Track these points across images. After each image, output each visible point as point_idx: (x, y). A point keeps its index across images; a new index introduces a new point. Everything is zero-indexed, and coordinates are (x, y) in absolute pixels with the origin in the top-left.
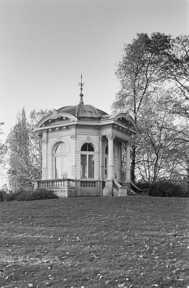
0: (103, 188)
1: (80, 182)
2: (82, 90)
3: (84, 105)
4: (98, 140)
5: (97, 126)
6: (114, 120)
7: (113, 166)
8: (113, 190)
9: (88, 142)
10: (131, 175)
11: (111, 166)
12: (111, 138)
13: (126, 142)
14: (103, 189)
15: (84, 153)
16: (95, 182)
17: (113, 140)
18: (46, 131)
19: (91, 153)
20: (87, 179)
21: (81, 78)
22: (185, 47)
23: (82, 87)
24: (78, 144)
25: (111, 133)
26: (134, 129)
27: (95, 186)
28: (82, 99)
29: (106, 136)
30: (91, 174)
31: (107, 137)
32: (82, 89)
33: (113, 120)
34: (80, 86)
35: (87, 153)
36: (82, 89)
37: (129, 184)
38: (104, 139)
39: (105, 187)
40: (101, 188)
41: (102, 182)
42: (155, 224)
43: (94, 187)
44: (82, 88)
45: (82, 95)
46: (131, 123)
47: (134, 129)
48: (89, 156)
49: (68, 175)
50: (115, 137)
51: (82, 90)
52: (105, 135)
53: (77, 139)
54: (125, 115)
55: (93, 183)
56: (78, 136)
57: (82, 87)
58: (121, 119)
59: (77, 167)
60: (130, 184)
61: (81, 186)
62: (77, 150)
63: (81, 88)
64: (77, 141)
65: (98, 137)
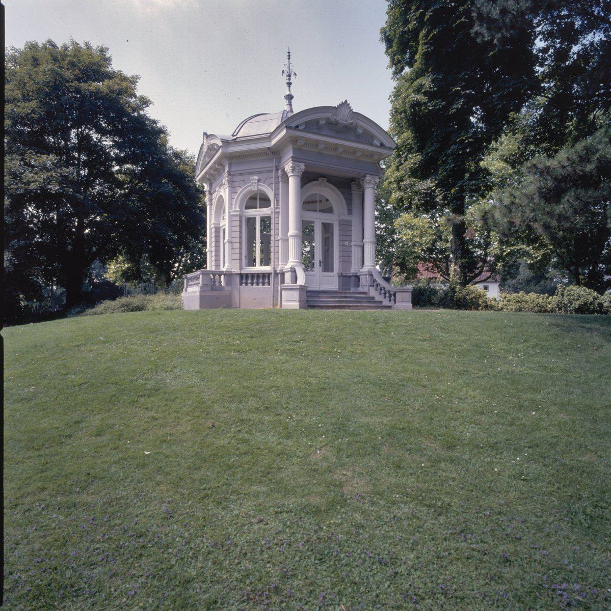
19: (266, 212)
20: (258, 268)
21: (289, 59)
27: (269, 284)
43: (266, 286)
57: (290, 79)
58: (322, 122)
61: (241, 284)
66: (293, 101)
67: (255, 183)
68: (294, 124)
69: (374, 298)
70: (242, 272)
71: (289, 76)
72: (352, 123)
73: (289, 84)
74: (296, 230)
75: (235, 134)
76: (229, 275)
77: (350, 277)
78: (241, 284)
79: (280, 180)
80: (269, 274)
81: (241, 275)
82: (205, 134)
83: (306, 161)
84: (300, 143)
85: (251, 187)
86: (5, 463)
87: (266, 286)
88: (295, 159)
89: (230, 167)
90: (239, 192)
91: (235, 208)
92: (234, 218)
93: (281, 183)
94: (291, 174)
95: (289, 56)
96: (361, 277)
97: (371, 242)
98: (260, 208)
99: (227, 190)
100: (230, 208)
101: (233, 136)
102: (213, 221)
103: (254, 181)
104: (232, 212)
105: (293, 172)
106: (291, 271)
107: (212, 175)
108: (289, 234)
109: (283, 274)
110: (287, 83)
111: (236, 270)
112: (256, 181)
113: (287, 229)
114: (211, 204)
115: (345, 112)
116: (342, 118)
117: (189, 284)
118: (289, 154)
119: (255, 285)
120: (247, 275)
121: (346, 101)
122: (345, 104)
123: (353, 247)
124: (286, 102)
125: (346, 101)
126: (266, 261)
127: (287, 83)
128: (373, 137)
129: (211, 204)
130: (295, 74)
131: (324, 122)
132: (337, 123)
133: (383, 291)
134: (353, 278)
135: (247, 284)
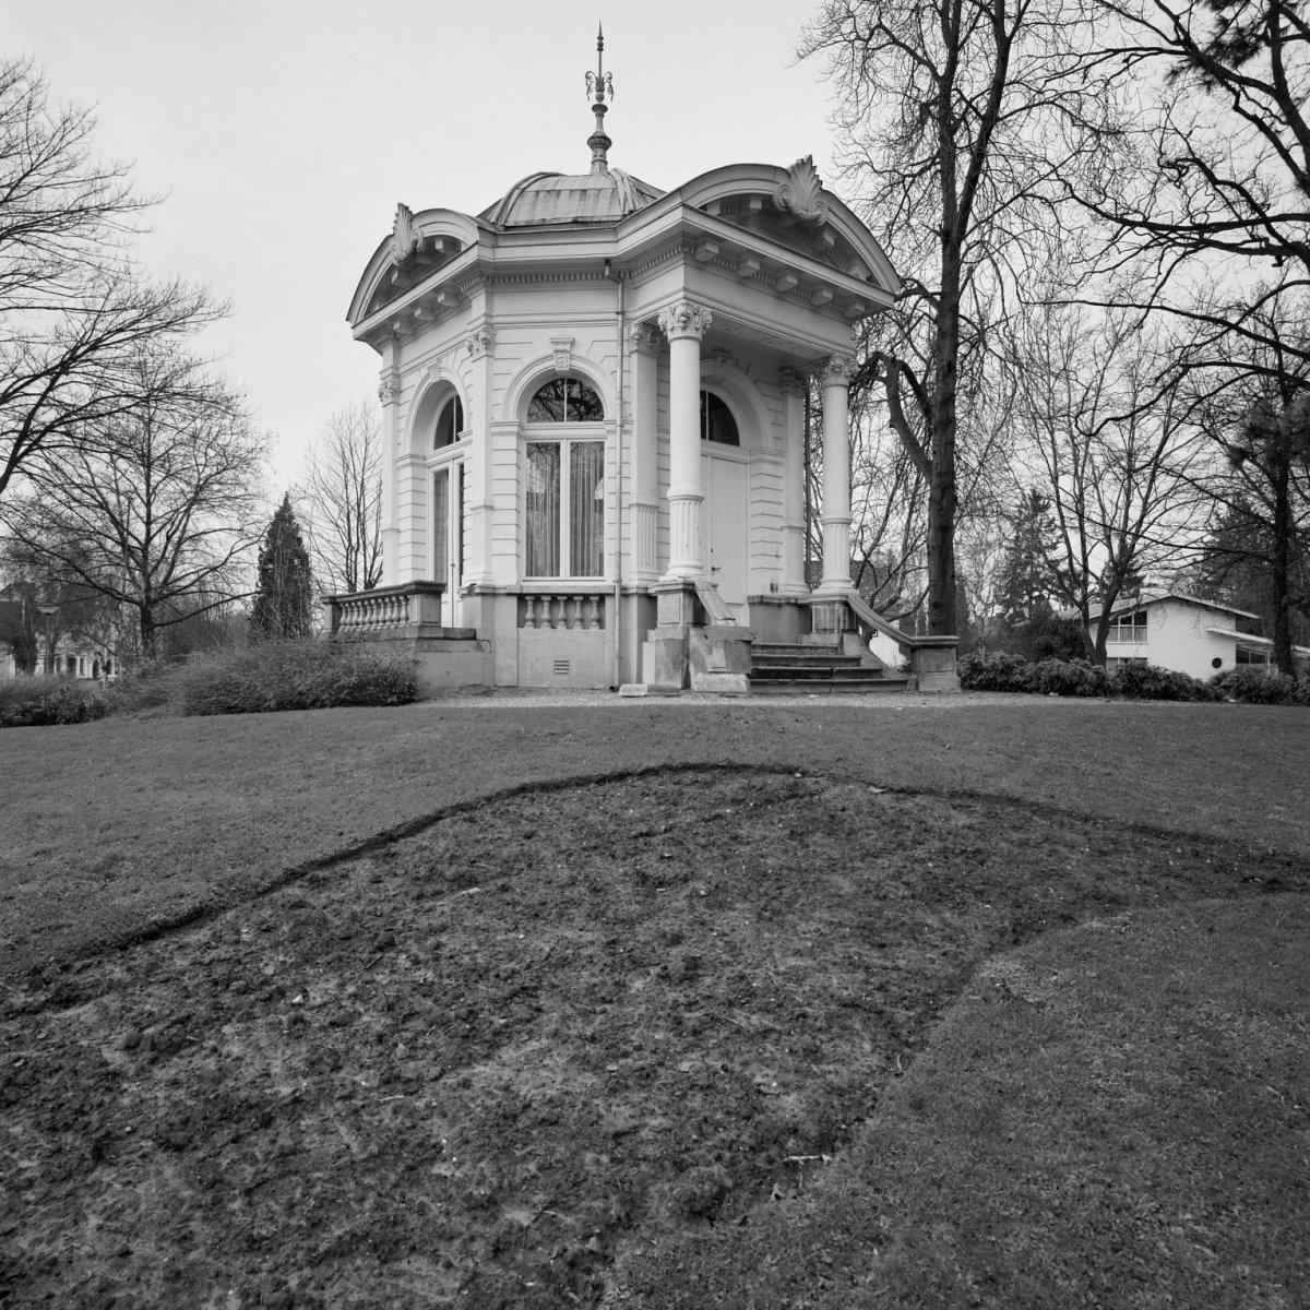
0: (646, 634)
1: (514, 601)
4: (614, 349)
5: (608, 261)
6: (684, 205)
7: (699, 499)
8: (687, 638)
9: (562, 365)
11: (684, 498)
12: (682, 325)
13: (821, 363)
14: (643, 638)
15: (546, 431)
16: (602, 598)
17: (698, 335)
19: (586, 430)
20: (565, 581)
24: (506, 382)
25: (682, 294)
26: (871, 280)
27: (600, 622)
30: (661, 558)
31: (660, 321)
33: (678, 200)
35: (566, 432)
36: (604, 109)
37: (837, 606)
38: (654, 342)
39: (654, 626)
40: (634, 635)
41: (640, 595)
43: (594, 628)
46: (839, 237)
47: (871, 280)
48: (576, 447)
50: (710, 318)
53: (500, 352)
54: (783, 181)
55: (542, 602)
56: (502, 336)
58: (756, 205)
59: (497, 517)
60: (846, 604)
61: (521, 623)
62: (498, 418)
64: (499, 366)
65: (612, 332)
73: (600, 110)
82: (404, 209)
83: (714, 304)
88: (689, 295)
92: (499, 442)
94: (679, 333)
105: (684, 328)
106: (684, 591)
108: (671, 493)
109: (650, 599)
110: (595, 108)
115: (804, 184)
116: (800, 200)
119: (561, 627)
120: (538, 598)
122: (806, 165)
124: (589, 153)
126: (578, 568)
127: (595, 108)
132: (788, 211)
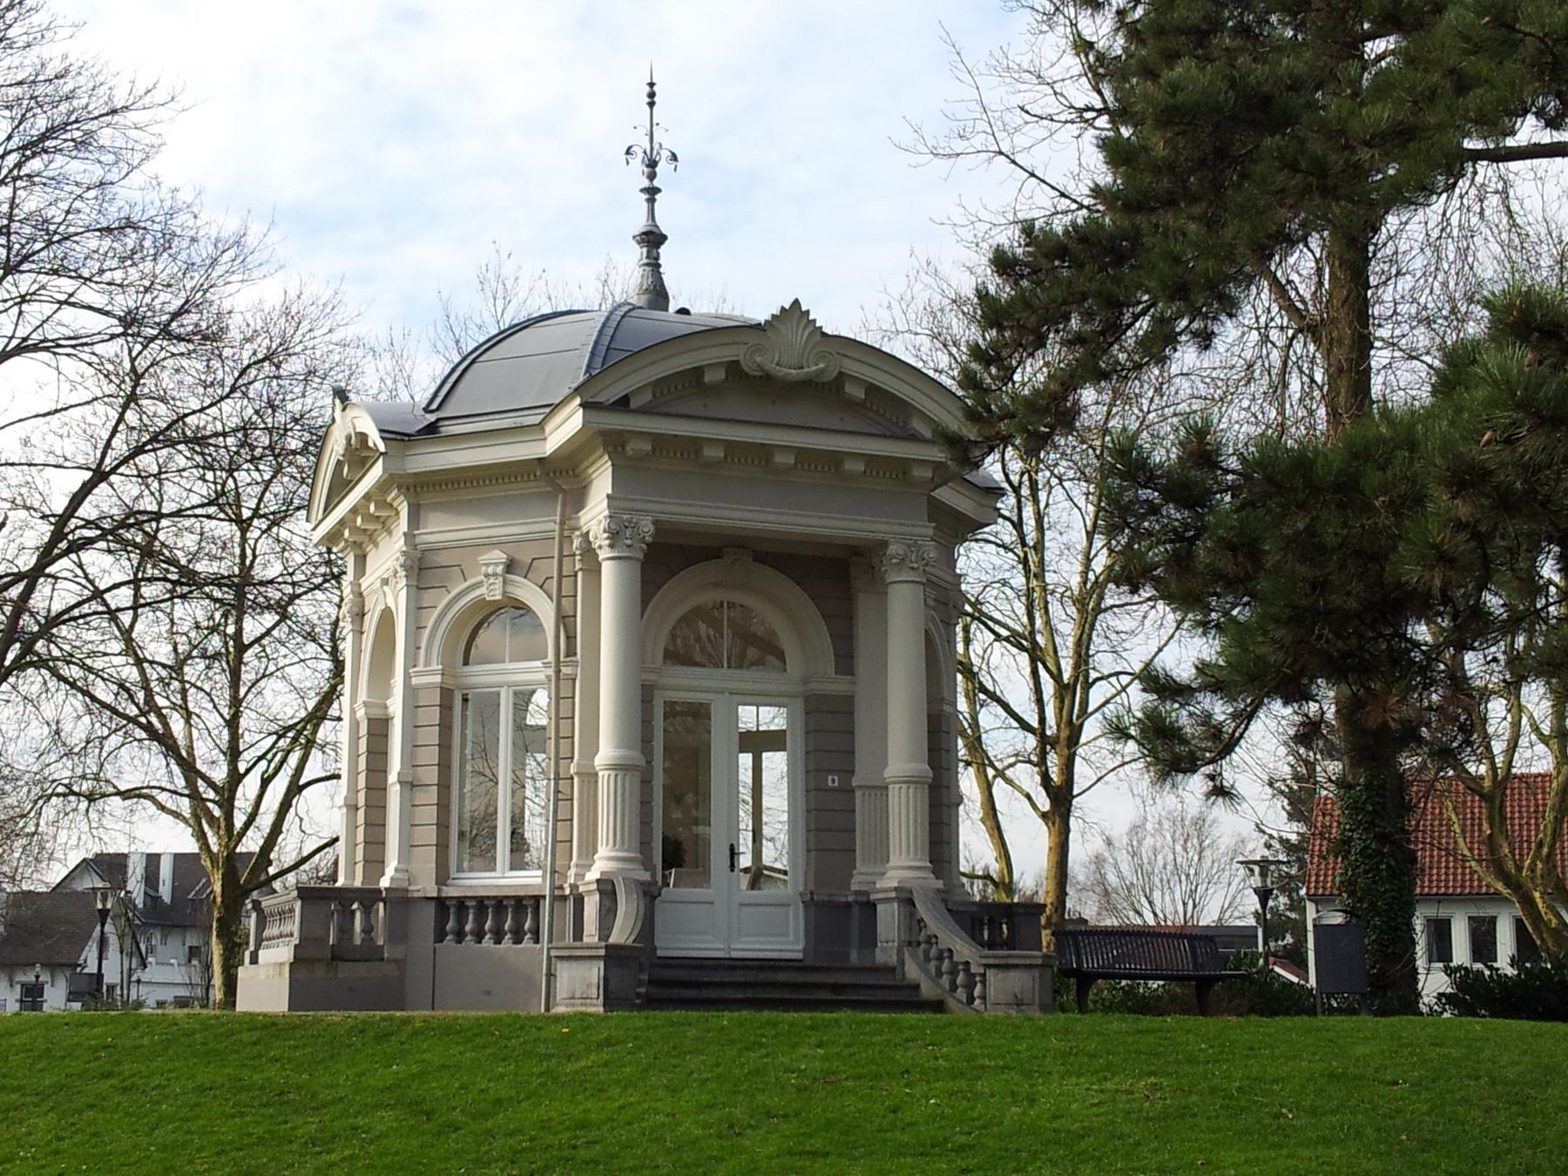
2: (652, 201)
3: (238, 1009)
10: (265, 1015)
18: (556, 904)
21: (652, 105)
22: (1057, 9)
23: (652, 176)
28: (654, 265)
29: (884, 544)
32: (658, 190)
34: (638, 166)
36: (658, 190)
42: (250, 1030)
44: (656, 183)
45: (653, 239)
48: (786, 935)
49: (152, 454)
51: (652, 201)
52: (880, 536)
57: (652, 176)
61: (440, 936)
63: (646, 183)
66: (663, 250)
67: (495, 575)
68: (612, 394)
69: (917, 987)
70: (450, 892)
71: (652, 164)
72: (823, 371)
73: (652, 192)
74: (627, 748)
75: (434, 406)
76: (400, 900)
77: (848, 905)
78: (440, 936)
79: (578, 566)
80: (537, 899)
81: (441, 903)
84: (632, 447)
85: (483, 590)
86: (785, 817)
87: (527, 942)
89: (415, 519)
90: (430, 624)
91: (427, 663)
93: (580, 574)
95: (652, 95)
96: (880, 908)
97: (911, 781)
98: (511, 661)
99: (403, 594)
100: (411, 661)
101: (427, 410)
102: (363, 695)
103: (490, 570)
104: (419, 674)
105: (611, 546)
107: (369, 518)
111: (426, 886)
112: (500, 569)
113: (592, 747)
114: (359, 633)
116: (782, 361)
117: (266, 933)
118: (602, 482)
121: (796, 303)
123: (858, 794)
125: (796, 303)
128: (903, 407)
129: (359, 633)
130: (674, 157)
131: (722, 376)
133: (946, 965)
134: (856, 910)
135: (460, 936)
